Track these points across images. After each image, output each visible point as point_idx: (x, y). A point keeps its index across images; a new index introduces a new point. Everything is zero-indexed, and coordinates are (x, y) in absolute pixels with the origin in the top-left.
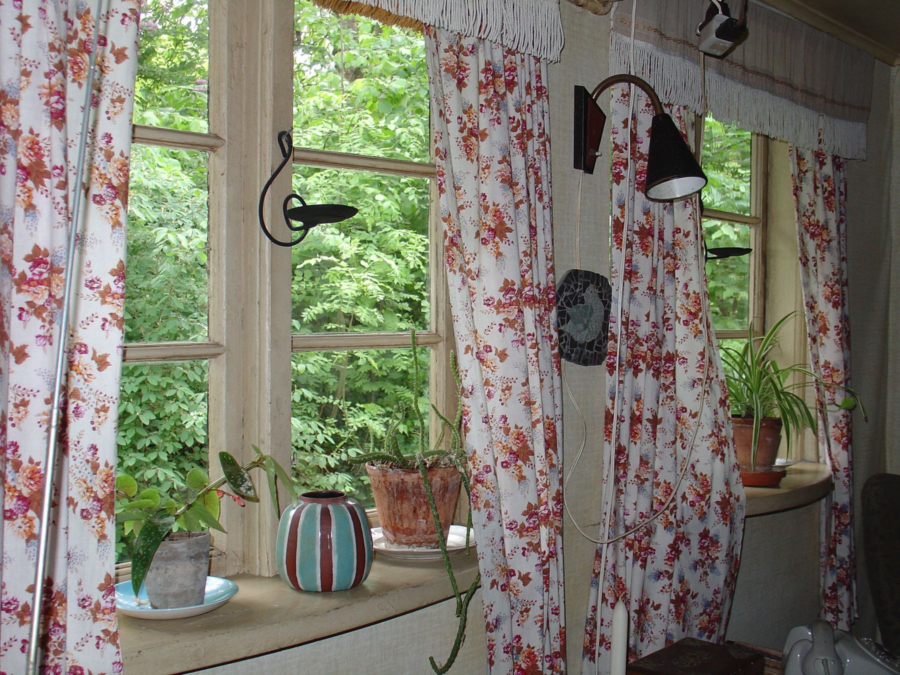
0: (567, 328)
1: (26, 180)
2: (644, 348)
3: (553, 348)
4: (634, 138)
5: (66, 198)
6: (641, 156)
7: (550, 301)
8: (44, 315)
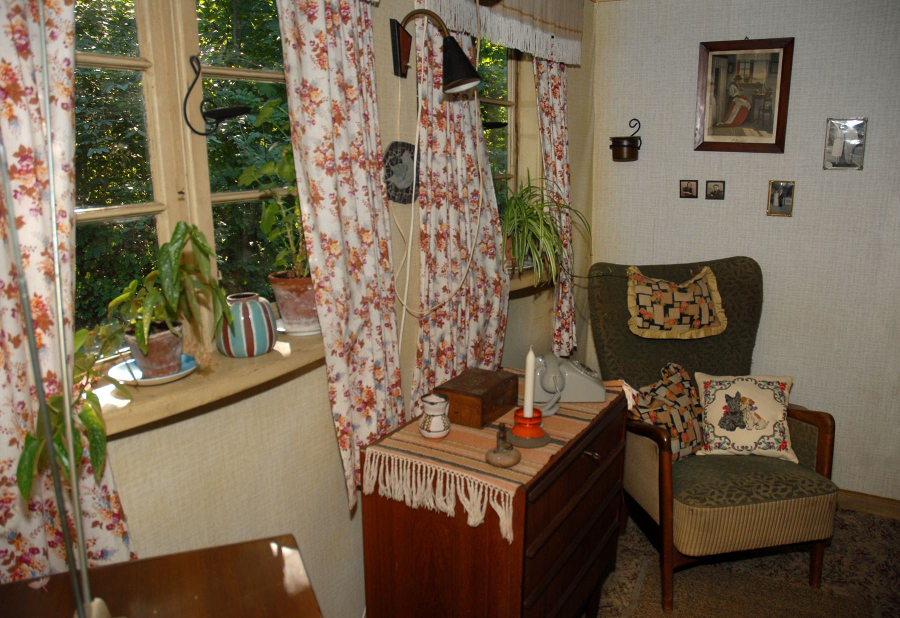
0: (392, 180)
1: (6, 97)
2: (444, 190)
3: (383, 194)
4: (431, 53)
5: (38, 110)
6: (437, 65)
7: (380, 163)
8: (34, 194)
